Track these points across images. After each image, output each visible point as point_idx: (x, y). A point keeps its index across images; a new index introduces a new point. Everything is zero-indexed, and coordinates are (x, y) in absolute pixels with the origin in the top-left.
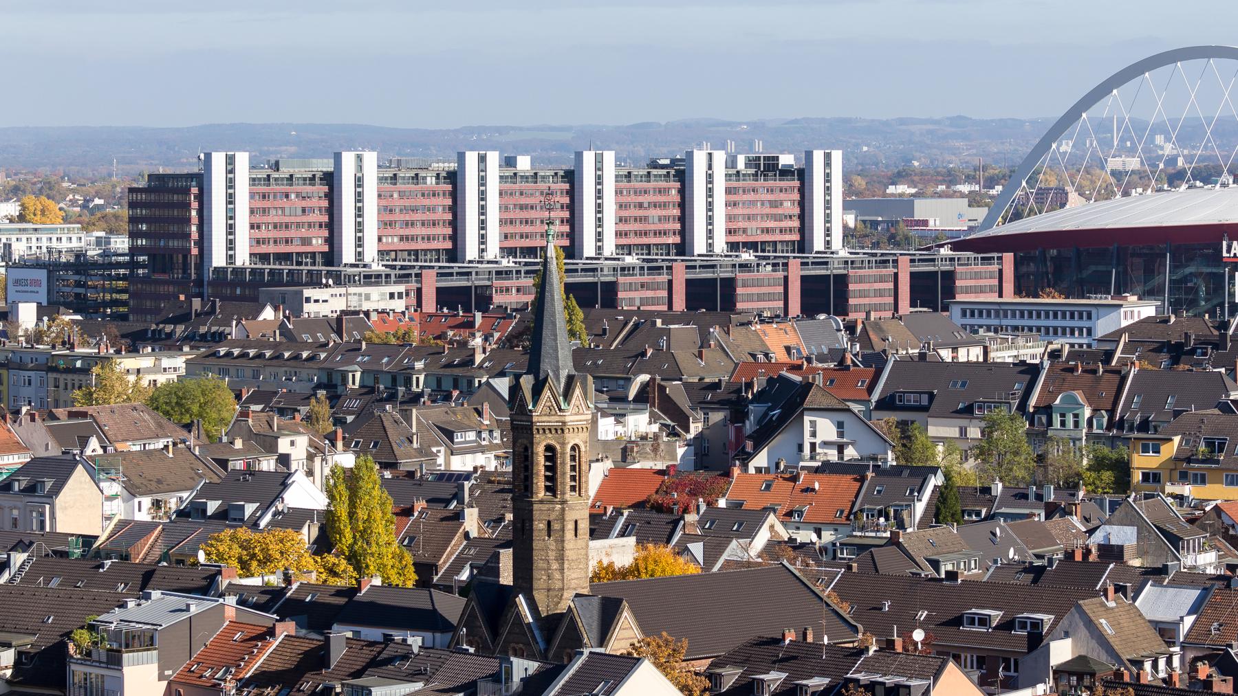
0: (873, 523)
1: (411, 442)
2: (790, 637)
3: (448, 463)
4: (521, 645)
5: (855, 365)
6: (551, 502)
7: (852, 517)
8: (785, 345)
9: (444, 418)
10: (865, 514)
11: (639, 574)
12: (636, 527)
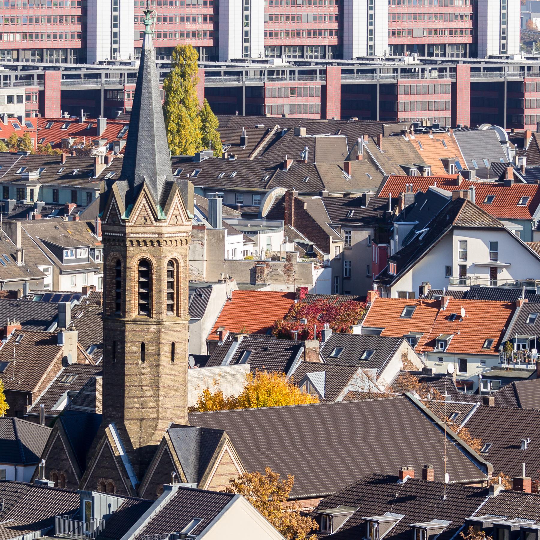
0: (524, 355)
1: (15, 259)
2: (409, 474)
3: (56, 283)
4: (110, 481)
5: (517, 180)
6: (145, 322)
7: (501, 348)
8: (444, 157)
9: (53, 233)
10: (515, 345)
11: (250, 405)
12: (252, 354)
